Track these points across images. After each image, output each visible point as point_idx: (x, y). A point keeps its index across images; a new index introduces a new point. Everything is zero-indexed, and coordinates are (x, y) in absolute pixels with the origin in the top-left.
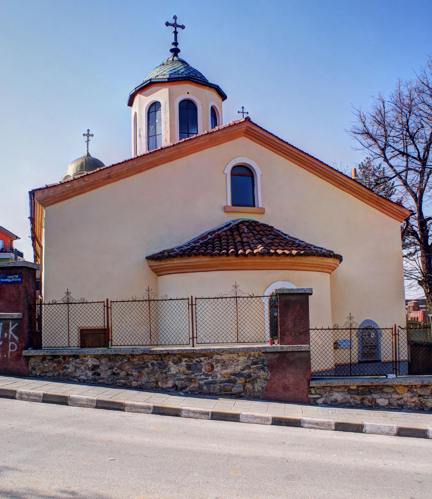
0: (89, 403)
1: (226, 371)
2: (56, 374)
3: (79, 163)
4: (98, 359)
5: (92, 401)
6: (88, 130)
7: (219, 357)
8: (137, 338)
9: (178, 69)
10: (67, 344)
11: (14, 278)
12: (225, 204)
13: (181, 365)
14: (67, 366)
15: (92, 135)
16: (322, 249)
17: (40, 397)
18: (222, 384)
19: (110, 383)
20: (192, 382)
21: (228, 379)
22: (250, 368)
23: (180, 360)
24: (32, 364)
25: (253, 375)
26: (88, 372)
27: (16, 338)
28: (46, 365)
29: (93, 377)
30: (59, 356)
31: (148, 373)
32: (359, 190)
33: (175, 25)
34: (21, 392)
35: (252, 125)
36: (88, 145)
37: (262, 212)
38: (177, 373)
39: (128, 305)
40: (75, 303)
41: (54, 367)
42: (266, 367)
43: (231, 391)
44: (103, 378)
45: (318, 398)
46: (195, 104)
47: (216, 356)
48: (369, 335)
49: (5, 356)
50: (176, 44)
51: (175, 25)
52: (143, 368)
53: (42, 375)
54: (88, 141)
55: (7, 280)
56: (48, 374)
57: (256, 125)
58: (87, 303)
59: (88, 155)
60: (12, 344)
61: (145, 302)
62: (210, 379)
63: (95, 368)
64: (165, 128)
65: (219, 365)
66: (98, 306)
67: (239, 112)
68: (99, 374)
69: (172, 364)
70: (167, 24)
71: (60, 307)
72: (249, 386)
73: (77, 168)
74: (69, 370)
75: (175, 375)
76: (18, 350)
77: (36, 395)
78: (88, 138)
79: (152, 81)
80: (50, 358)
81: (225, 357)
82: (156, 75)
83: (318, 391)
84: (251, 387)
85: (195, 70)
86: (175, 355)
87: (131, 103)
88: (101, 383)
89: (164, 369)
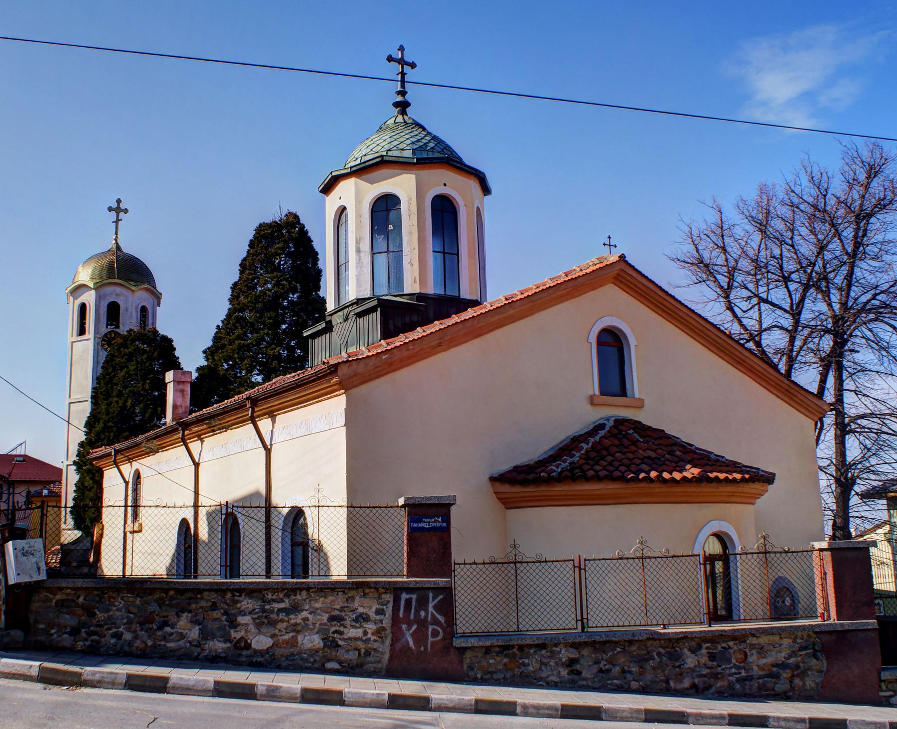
0: (635, 715)
1: (765, 661)
2: (508, 675)
3: (105, 261)
4: (576, 648)
5: (638, 711)
6: (119, 201)
7: (754, 641)
8: (626, 616)
9: (424, 141)
10: (515, 627)
11: (435, 521)
12: (591, 393)
13: (701, 654)
14: (526, 661)
15: (126, 211)
16: (758, 469)
17: (557, 710)
18: (761, 681)
19: (597, 685)
20: (719, 679)
21: (768, 672)
22: (796, 656)
23: (700, 647)
24: (468, 660)
25: (801, 665)
26: (561, 670)
27: (441, 619)
28: (491, 661)
29: (570, 677)
30: (513, 647)
31: (654, 668)
32: (765, 373)
33: (402, 62)
34: (525, 704)
35: (628, 267)
36: (117, 228)
37: (640, 405)
38: (696, 666)
39: (606, 565)
40: (527, 562)
41: (505, 664)
42: (819, 654)
43: (773, 689)
44: (585, 679)
45: (892, 696)
46: (453, 204)
47: (750, 639)
48: (783, 602)
49: (422, 648)
50: (403, 93)
51: (402, 62)
52: (647, 660)
53: (485, 677)
54: (117, 221)
55: (423, 525)
56: (495, 676)
57: (633, 267)
58: (546, 561)
59: (118, 248)
60: (433, 630)
61: (636, 560)
62: (743, 673)
63: (572, 662)
64: (409, 241)
65: (754, 651)
66: (564, 566)
67: (615, 246)
68: (579, 673)
69: (689, 653)
70: (390, 59)
71: (503, 569)
72: (797, 682)
73: (101, 272)
74: (531, 668)
75: (693, 670)
76: (444, 639)
77: (549, 708)
78: (118, 216)
79: (385, 158)
80: (497, 649)
81: (764, 640)
82: (387, 147)
83: (890, 686)
84: (801, 683)
85: (447, 145)
86: (692, 639)
87: (327, 189)
88: (583, 685)
89: (676, 661)
